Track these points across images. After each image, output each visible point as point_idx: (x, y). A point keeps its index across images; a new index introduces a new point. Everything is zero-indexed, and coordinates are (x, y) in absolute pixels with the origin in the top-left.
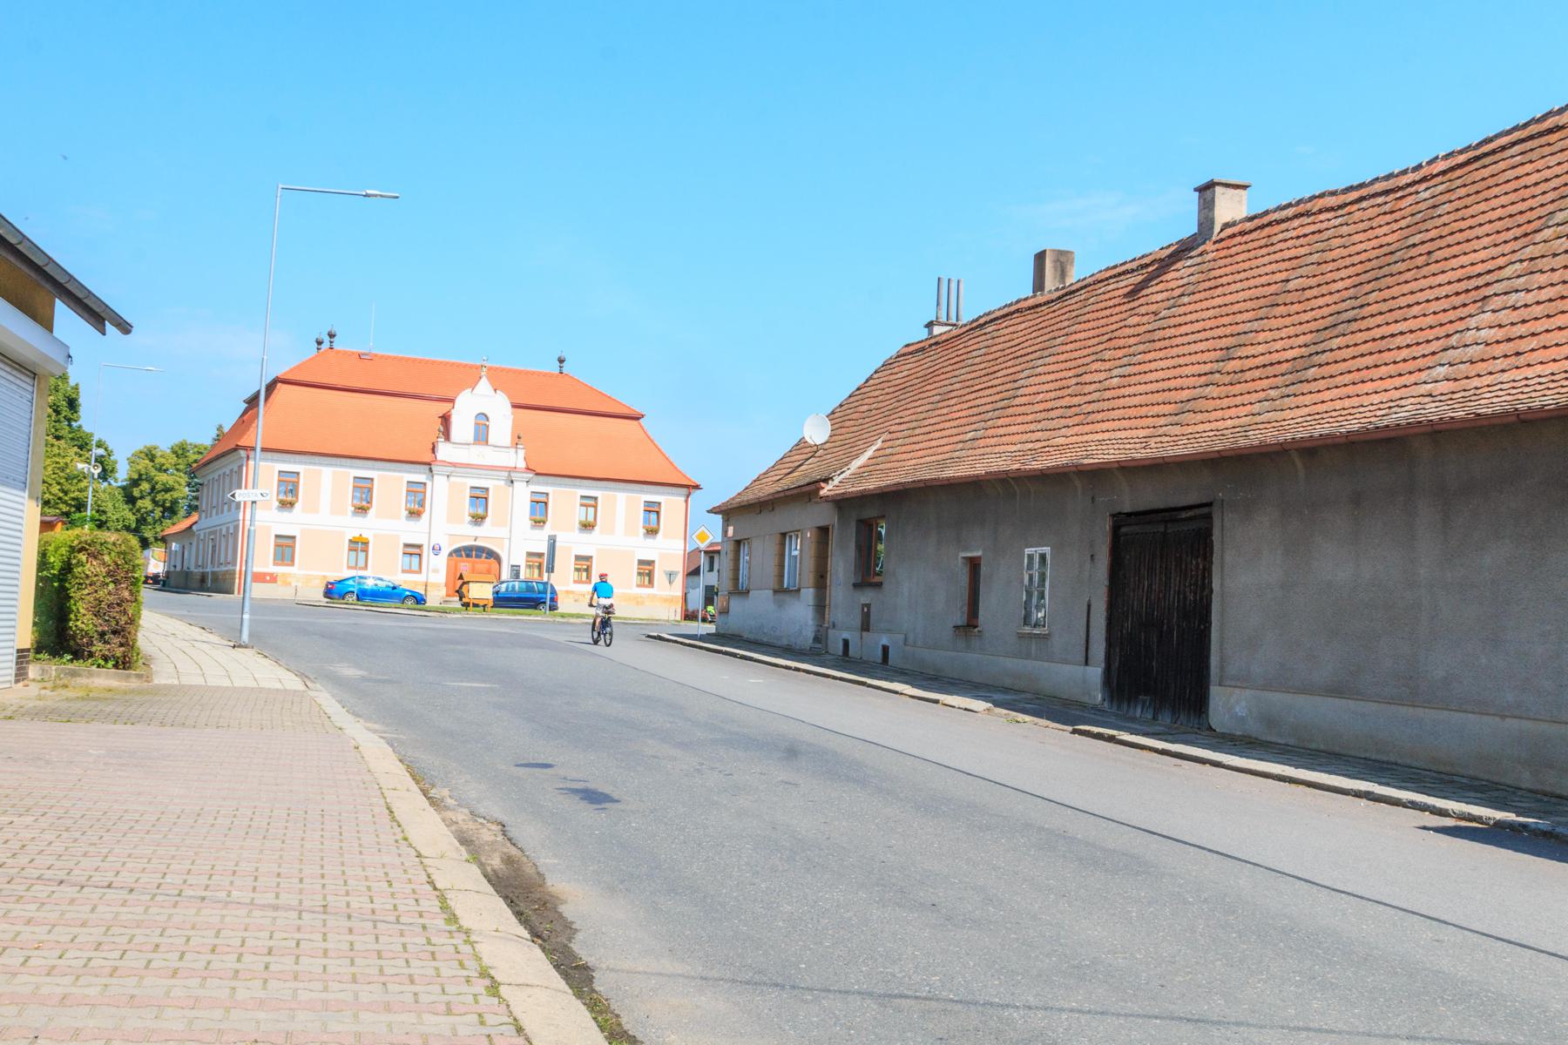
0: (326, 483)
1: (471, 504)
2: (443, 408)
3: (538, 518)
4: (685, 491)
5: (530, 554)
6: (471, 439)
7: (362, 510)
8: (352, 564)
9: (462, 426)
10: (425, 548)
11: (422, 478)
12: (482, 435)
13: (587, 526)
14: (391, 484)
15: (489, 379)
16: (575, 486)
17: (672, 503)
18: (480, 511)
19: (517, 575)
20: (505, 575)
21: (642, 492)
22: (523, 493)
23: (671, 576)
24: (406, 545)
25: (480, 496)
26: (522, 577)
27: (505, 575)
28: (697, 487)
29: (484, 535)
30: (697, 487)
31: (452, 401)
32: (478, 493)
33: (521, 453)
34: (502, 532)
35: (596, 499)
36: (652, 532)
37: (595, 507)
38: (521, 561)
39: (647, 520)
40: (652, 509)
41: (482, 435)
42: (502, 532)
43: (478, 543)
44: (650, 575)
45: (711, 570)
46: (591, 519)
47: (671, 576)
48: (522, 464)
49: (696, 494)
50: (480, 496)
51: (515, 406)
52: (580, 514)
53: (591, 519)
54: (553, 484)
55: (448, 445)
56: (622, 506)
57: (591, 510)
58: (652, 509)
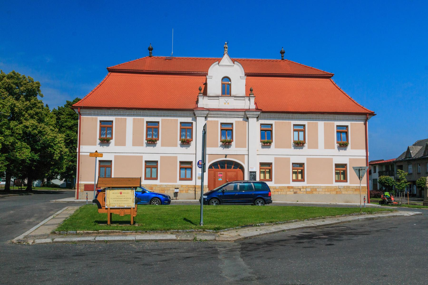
0: (130, 126)
1: (222, 134)
2: (200, 80)
3: (266, 140)
4: (364, 117)
5: (262, 164)
6: (219, 92)
7: (152, 142)
8: (148, 176)
9: (214, 86)
10: (194, 164)
11: (189, 120)
12: (226, 90)
13: (299, 144)
14: (170, 125)
15: (228, 54)
16: (289, 119)
17: (356, 128)
18: (228, 139)
19: (254, 178)
20: (247, 178)
21: (335, 120)
22: (254, 126)
23: (359, 170)
24: (181, 163)
25: (227, 130)
26: (258, 179)
27: (247, 178)
28: (372, 114)
29: (233, 152)
30: (372, 114)
31: (206, 75)
32: (253, 174)
33: (253, 100)
34: (242, 151)
35: (304, 126)
36: (343, 145)
37: (304, 131)
38: (256, 168)
39: (339, 138)
40: (342, 132)
41: (226, 90)
42: (242, 151)
43: (227, 159)
44: (344, 173)
45: (375, 172)
46: (301, 139)
47: (359, 170)
48: (253, 107)
49: (372, 119)
50: (227, 130)
51: (247, 75)
52: (294, 136)
53: (301, 139)
54: (274, 119)
55: (206, 98)
56: (322, 130)
57: (301, 134)
58: (342, 132)
